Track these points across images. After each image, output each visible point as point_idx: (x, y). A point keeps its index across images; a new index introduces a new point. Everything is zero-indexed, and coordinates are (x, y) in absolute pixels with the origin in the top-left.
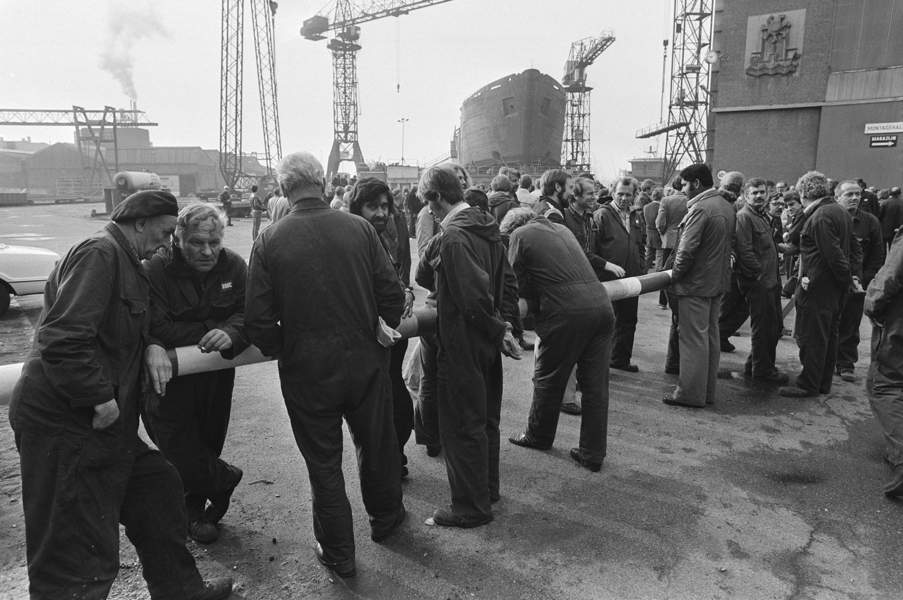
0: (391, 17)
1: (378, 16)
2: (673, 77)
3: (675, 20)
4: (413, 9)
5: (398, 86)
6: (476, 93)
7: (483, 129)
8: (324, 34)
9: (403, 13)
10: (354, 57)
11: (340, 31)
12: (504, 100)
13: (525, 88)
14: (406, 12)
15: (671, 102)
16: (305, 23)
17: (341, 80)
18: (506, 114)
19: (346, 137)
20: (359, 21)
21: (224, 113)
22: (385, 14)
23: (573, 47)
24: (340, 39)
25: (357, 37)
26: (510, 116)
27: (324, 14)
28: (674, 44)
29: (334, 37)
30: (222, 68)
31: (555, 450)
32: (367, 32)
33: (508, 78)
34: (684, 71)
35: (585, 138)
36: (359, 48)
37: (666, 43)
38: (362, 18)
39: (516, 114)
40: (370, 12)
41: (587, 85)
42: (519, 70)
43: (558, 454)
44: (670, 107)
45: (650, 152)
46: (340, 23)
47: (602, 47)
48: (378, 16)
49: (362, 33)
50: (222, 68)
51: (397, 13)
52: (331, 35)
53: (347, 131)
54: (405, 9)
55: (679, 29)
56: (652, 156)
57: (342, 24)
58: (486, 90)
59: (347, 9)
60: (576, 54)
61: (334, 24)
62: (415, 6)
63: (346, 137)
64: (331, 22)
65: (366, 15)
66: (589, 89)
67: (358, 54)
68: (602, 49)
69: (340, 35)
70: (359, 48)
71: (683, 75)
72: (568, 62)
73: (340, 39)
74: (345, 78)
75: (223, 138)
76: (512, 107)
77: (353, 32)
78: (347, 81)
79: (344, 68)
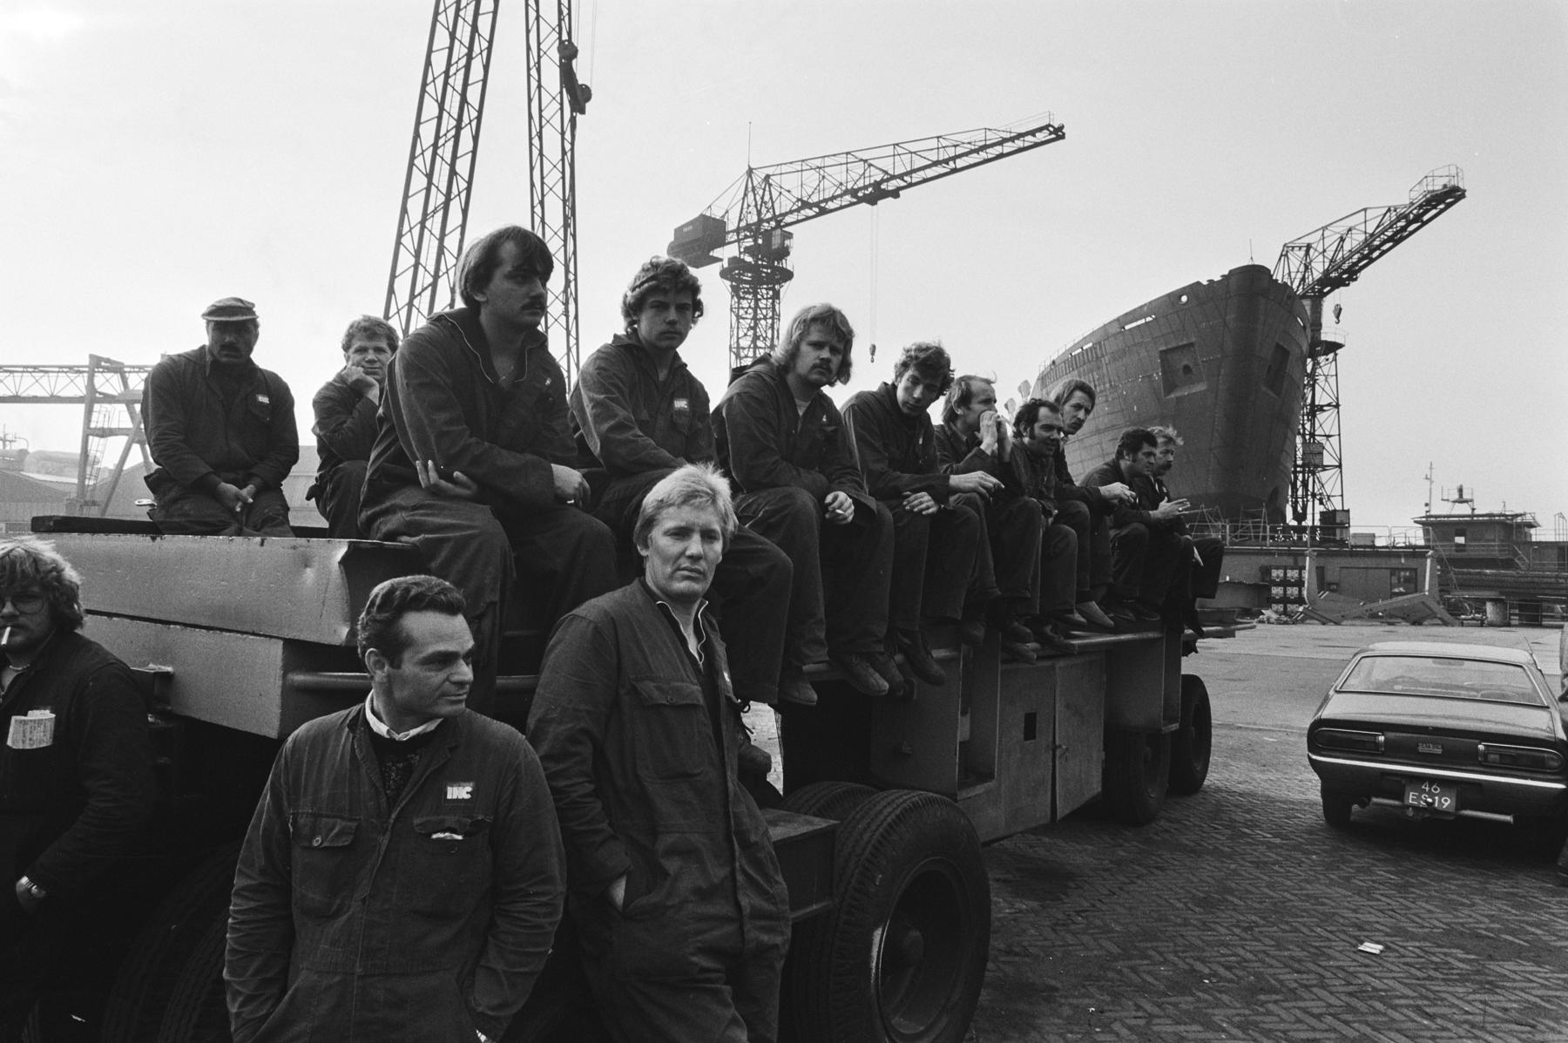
0: (864, 205)
1: (831, 205)
4: (911, 185)
6: (1079, 345)
8: (716, 253)
10: (776, 295)
11: (749, 242)
12: (1164, 354)
13: (1231, 317)
14: (895, 194)
16: (678, 231)
17: (745, 342)
18: (1170, 386)
20: (788, 219)
21: (532, 15)
22: (848, 199)
24: (748, 259)
25: (784, 252)
26: (1178, 394)
27: (717, 213)
29: (737, 254)
30: (529, 48)
33: (1176, 295)
35: (1328, 460)
36: (788, 275)
38: (798, 210)
39: (1200, 387)
40: (815, 199)
42: (1212, 271)
45: (1461, 500)
46: (748, 227)
48: (831, 205)
49: (795, 245)
50: (529, 48)
51: (876, 194)
52: (727, 252)
54: (892, 185)
56: (1464, 510)
57: (754, 230)
59: (767, 198)
61: (738, 231)
62: (916, 177)
64: (731, 226)
65: (806, 205)
66: (1333, 347)
68: (1397, 239)
69: (747, 250)
70: (788, 275)
73: (748, 259)
74: (756, 338)
75: (534, 72)
76: (1187, 369)
77: (776, 242)
78: (760, 344)
79: (755, 318)
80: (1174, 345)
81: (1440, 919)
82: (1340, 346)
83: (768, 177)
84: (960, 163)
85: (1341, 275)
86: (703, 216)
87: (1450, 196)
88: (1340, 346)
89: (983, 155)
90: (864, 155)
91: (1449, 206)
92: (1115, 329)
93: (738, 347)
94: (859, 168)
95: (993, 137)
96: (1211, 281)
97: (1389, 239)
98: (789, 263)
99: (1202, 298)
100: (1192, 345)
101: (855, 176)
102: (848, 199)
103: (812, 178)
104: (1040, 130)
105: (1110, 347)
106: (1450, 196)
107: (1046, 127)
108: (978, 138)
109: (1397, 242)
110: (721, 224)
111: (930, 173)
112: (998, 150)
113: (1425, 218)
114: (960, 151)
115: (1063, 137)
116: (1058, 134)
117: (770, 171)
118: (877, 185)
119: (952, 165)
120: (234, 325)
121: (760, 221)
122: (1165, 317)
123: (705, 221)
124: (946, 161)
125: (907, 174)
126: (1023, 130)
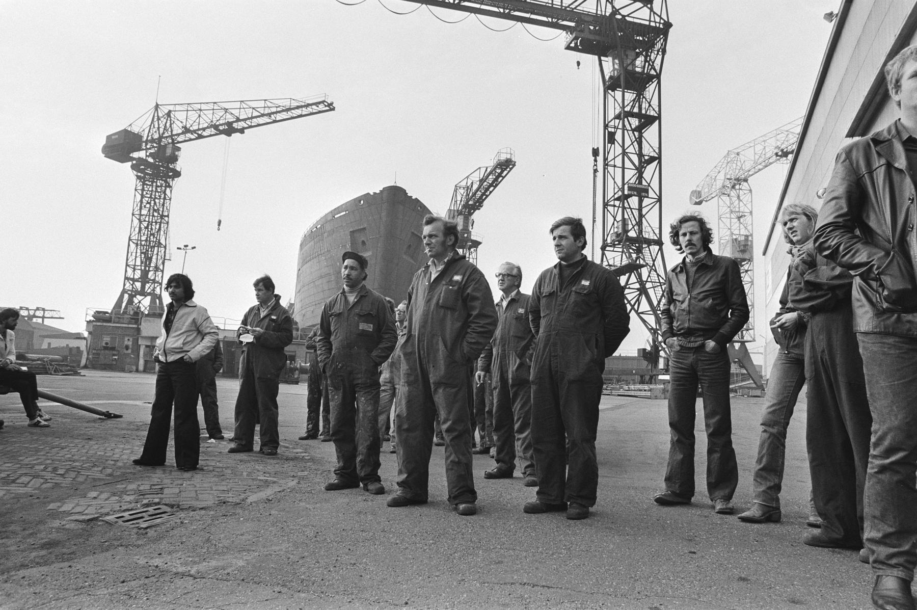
0: (223, 136)
2: (605, 205)
3: (606, 126)
4: (251, 127)
5: (220, 222)
7: (321, 277)
9: (237, 131)
12: (352, 233)
13: (384, 214)
14: (242, 131)
15: (604, 240)
16: (109, 137)
19: (143, 287)
20: (179, 139)
23: (456, 191)
24: (151, 160)
25: (174, 159)
27: (135, 129)
28: (605, 159)
31: (432, 503)
32: (189, 156)
33: (358, 200)
34: (626, 193)
36: (177, 174)
37: (595, 152)
40: (195, 128)
41: (473, 238)
42: (376, 188)
43: (434, 504)
44: (603, 248)
47: (496, 180)
51: (229, 130)
53: (384, 452)
54: (241, 125)
55: (611, 138)
58: (330, 218)
60: (459, 198)
63: (143, 287)
67: (176, 183)
68: (495, 184)
69: (151, 155)
70: (177, 174)
71: (624, 198)
72: (450, 210)
73: (151, 160)
76: (363, 242)
77: (169, 151)
80: (356, 228)
81: (362, 505)
82: (480, 243)
83: (170, 111)
84: (279, 117)
85: (473, 203)
86: (125, 131)
87: (506, 165)
88: (480, 243)
89: (290, 114)
90: (226, 106)
91: (511, 169)
92: (330, 218)
93: (141, 215)
94: (222, 113)
95: (294, 104)
96: (375, 193)
97: (491, 185)
98: (179, 166)
99: (366, 204)
100: (365, 229)
101: (221, 118)
102: (213, 131)
103: (193, 116)
104: (320, 103)
105: (328, 227)
106: (506, 165)
107: (323, 102)
108: (287, 104)
109: (495, 187)
110: (138, 137)
111: (261, 120)
112: (298, 112)
113: (504, 174)
114: (279, 109)
115: (333, 109)
116: (331, 107)
117: (171, 108)
118: (230, 124)
119: (273, 117)
120: (265, 286)
121: (161, 138)
122: (353, 212)
123: (126, 133)
124: (269, 115)
125: (249, 118)
126: (310, 102)
